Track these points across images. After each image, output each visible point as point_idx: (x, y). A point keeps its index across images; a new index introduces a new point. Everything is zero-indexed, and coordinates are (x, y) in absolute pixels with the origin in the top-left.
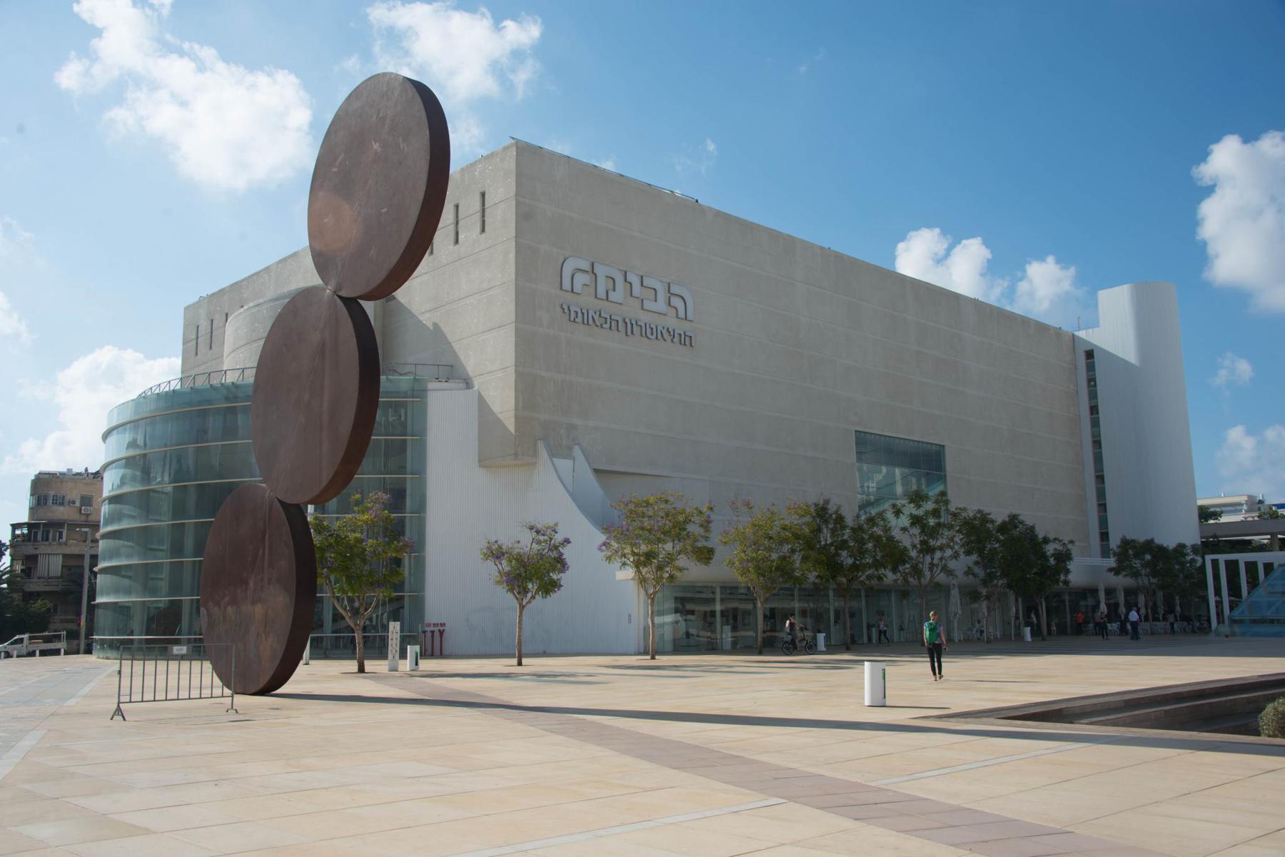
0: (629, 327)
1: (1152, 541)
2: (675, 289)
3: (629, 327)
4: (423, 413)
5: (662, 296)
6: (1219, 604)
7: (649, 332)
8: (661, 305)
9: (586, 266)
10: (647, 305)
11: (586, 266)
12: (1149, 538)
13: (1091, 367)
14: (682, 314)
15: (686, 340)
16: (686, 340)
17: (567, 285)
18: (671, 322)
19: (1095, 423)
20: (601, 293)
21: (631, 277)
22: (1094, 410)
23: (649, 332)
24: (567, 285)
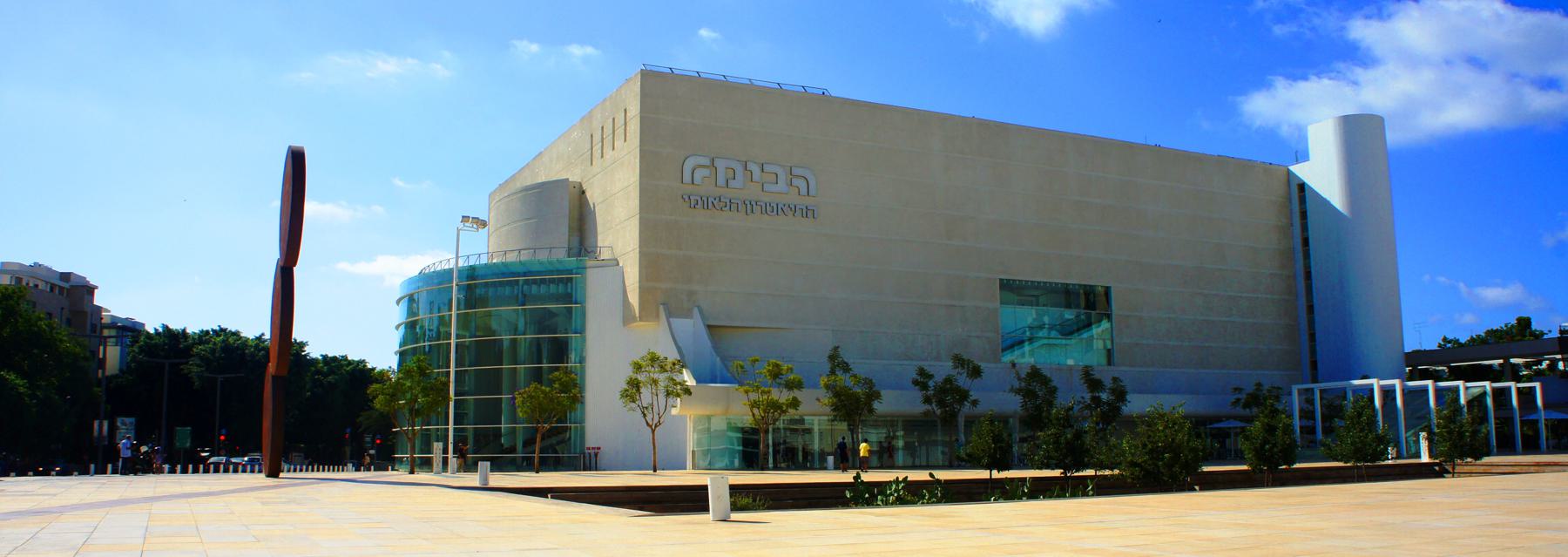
0: (749, 207)
1: (90, 290)
2: (796, 171)
3: (749, 207)
4: (584, 280)
5: (782, 177)
6: (445, 451)
7: (778, 209)
8: (782, 186)
9: (707, 162)
10: (767, 187)
11: (707, 162)
12: (93, 282)
13: (1302, 200)
14: (804, 191)
15: (808, 212)
16: (808, 212)
17: (687, 178)
18: (793, 198)
19: (1307, 255)
20: (721, 181)
21: (751, 166)
22: (1306, 242)
23: (778, 209)
24: (687, 178)
